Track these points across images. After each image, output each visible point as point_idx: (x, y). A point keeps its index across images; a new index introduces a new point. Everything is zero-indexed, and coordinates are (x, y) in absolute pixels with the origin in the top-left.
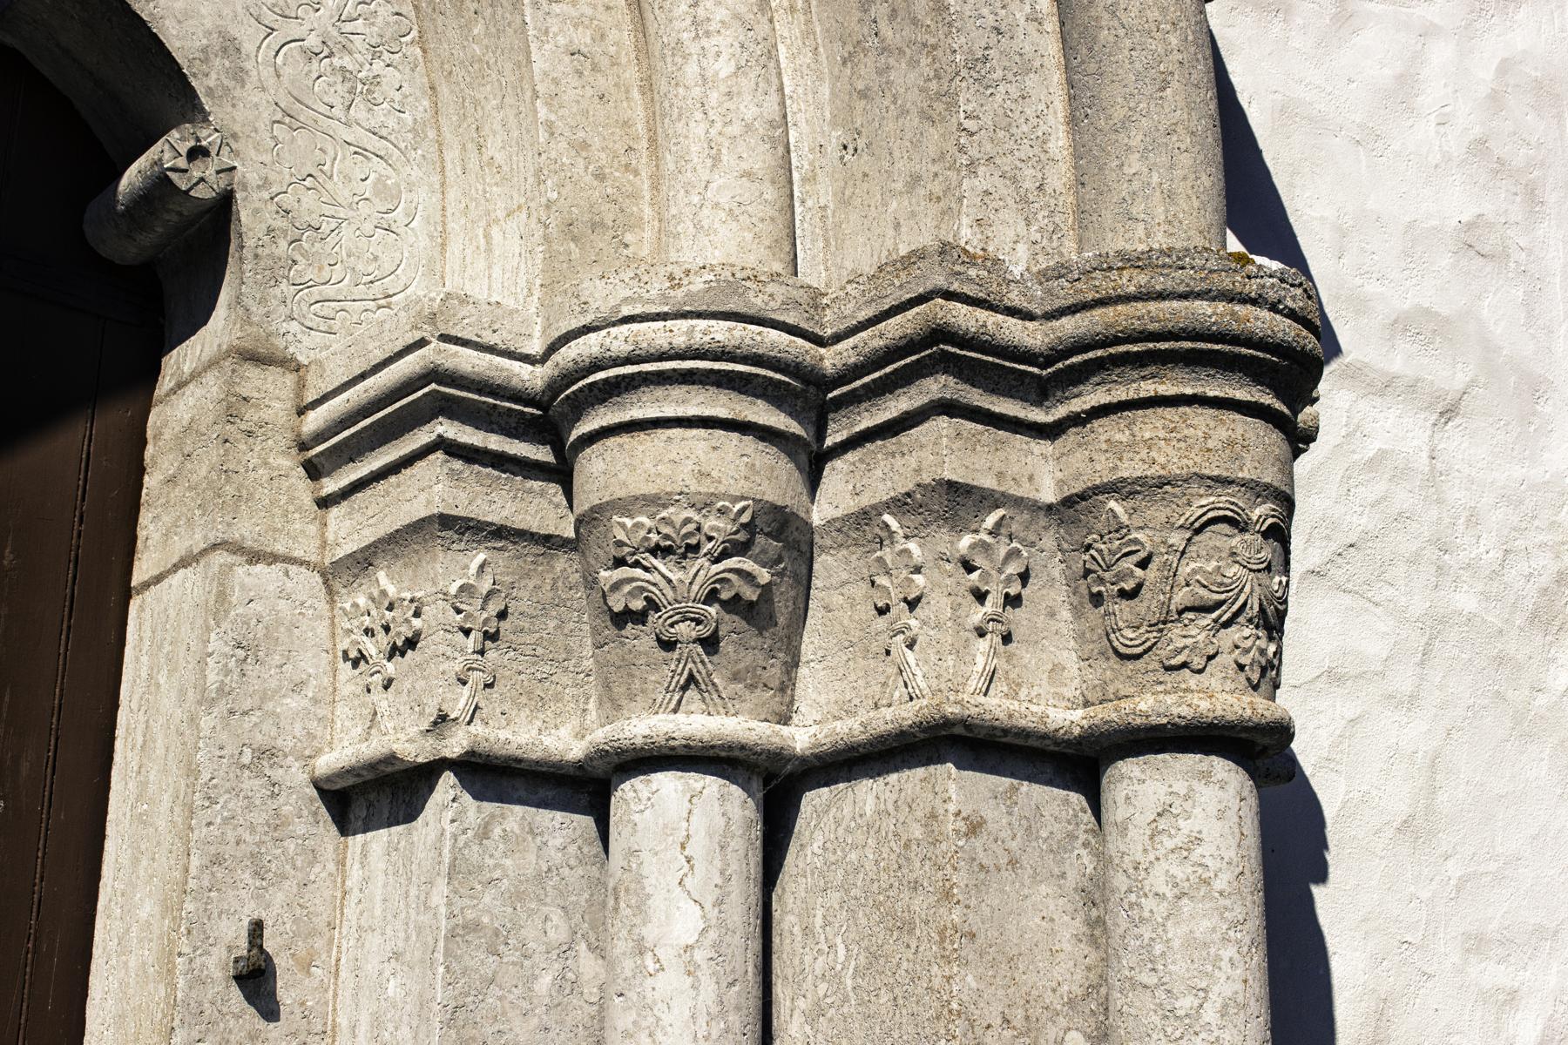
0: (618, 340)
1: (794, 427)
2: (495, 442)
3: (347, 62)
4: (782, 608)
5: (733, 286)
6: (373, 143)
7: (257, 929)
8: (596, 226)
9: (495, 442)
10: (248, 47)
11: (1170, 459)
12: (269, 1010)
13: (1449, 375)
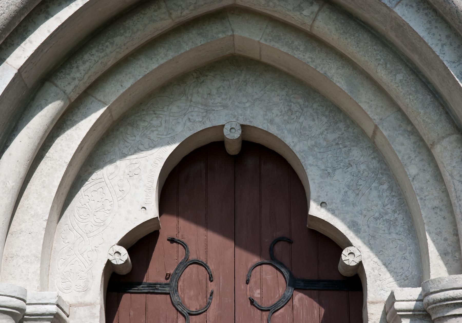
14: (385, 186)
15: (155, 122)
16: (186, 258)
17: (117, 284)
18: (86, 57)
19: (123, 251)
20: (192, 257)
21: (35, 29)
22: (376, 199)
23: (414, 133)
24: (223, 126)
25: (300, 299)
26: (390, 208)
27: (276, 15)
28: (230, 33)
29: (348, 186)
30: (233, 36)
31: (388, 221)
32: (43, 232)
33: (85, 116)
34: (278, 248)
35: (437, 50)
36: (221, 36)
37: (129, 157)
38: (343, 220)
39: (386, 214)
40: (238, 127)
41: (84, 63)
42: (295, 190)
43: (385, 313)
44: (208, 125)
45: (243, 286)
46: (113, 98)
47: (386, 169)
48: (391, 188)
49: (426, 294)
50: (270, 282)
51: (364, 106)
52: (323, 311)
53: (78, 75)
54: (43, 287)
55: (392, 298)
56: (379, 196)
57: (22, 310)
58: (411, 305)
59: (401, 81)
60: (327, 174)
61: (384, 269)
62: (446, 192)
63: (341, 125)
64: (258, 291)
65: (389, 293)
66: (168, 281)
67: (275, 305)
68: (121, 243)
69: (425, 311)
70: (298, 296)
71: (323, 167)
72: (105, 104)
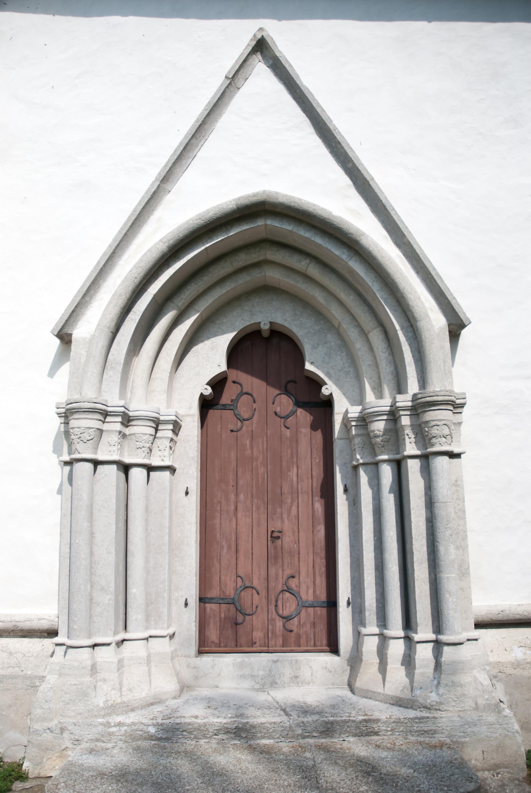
14: (344, 354)
15: (225, 320)
16: (242, 391)
17: (206, 405)
18: (189, 287)
19: (209, 388)
20: (245, 390)
21: (162, 274)
22: (340, 360)
23: (359, 326)
24: (260, 322)
25: (301, 412)
26: (347, 365)
27: (288, 265)
28: (263, 274)
29: (326, 354)
30: (265, 276)
31: (345, 372)
32: (168, 379)
33: (188, 318)
34: (289, 386)
35: (370, 284)
36: (259, 275)
37: (211, 339)
38: (323, 371)
39: (345, 368)
40: (268, 323)
41: (187, 290)
42: (297, 355)
43: (343, 419)
44: (253, 322)
45: (271, 405)
46: (202, 309)
47: (345, 345)
48: (347, 355)
49: (364, 409)
50: (285, 403)
51: (333, 312)
52: (312, 418)
53: (184, 297)
54: (169, 406)
55: (347, 412)
56: (341, 359)
57: (158, 419)
58: (357, 415)
59: (352, 300)
60: (314, 347)
61: (343, 396)
62: (375, 357)
63: (322, 322)
64: (279, 408)
65: (345, 409)
66: (232, 403)
67: (288, 415)
68: (207, 384)
69: (363, 418)
70: (300, 411)
71: (312, 344)
72: (198, 312)
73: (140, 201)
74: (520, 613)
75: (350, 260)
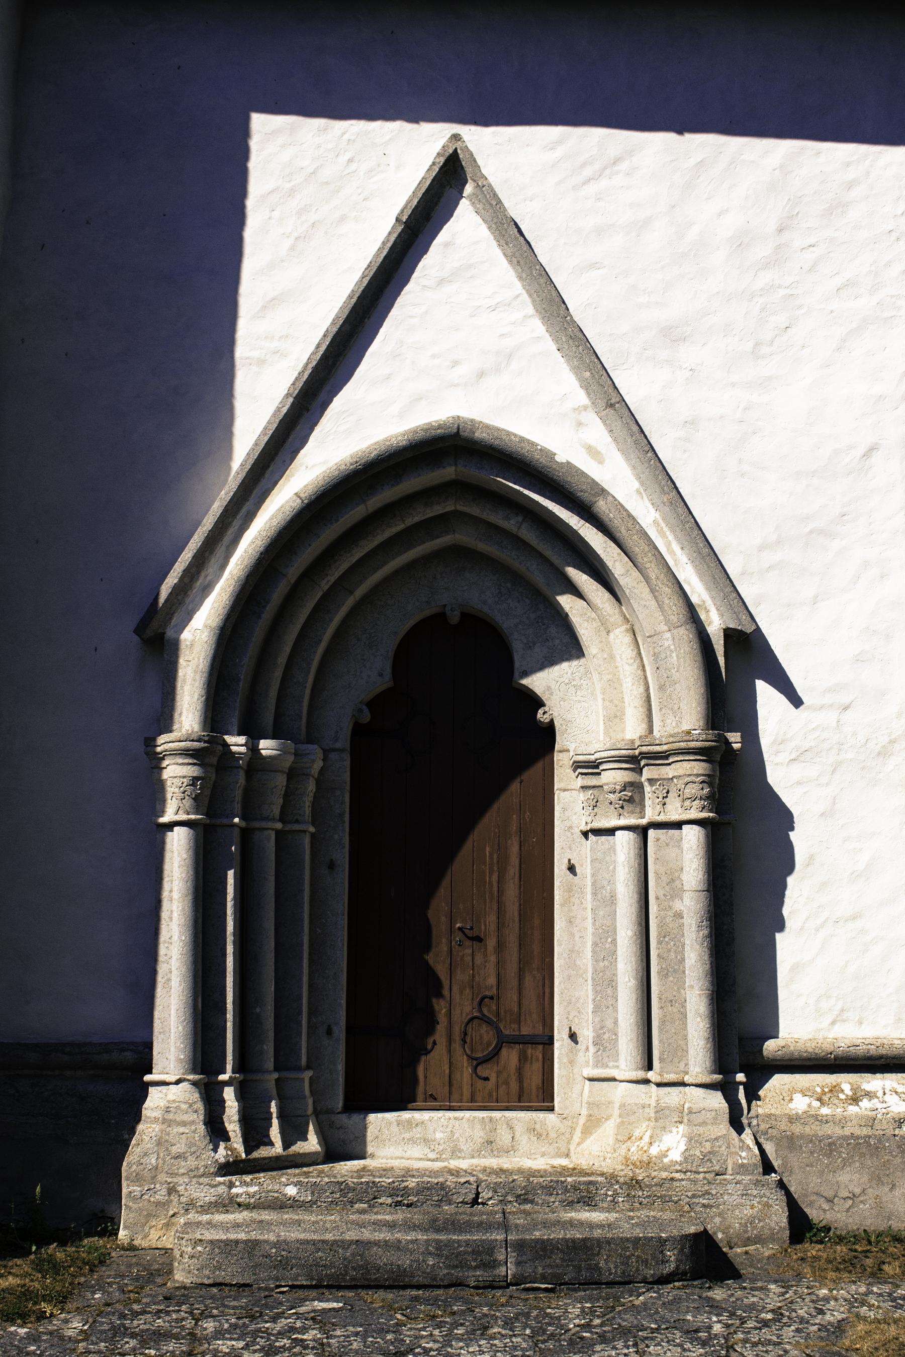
0: (597, 755)
1: (632, 766)
2: (590, 771)
3: (575, 683)
4: (637, 798)
5: (614, 744)
6: (583, 699)
7: (569, 860)
8: (616, 717)
9: (590, 771)
10: (553, 687)
11: (681, 772)
12: (575, 874)
13: (845, 699)
73: (265, 428)
74: (810, 1050)
75: (308, 775)
